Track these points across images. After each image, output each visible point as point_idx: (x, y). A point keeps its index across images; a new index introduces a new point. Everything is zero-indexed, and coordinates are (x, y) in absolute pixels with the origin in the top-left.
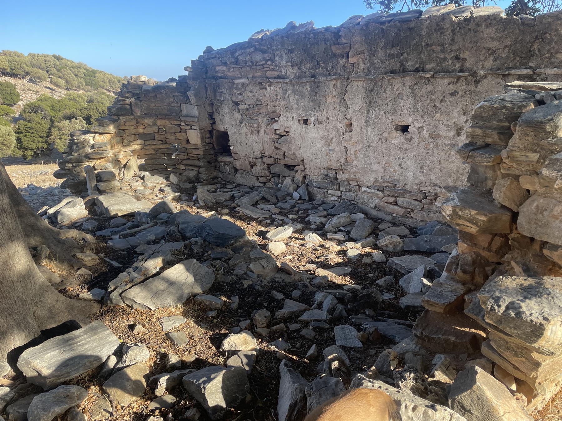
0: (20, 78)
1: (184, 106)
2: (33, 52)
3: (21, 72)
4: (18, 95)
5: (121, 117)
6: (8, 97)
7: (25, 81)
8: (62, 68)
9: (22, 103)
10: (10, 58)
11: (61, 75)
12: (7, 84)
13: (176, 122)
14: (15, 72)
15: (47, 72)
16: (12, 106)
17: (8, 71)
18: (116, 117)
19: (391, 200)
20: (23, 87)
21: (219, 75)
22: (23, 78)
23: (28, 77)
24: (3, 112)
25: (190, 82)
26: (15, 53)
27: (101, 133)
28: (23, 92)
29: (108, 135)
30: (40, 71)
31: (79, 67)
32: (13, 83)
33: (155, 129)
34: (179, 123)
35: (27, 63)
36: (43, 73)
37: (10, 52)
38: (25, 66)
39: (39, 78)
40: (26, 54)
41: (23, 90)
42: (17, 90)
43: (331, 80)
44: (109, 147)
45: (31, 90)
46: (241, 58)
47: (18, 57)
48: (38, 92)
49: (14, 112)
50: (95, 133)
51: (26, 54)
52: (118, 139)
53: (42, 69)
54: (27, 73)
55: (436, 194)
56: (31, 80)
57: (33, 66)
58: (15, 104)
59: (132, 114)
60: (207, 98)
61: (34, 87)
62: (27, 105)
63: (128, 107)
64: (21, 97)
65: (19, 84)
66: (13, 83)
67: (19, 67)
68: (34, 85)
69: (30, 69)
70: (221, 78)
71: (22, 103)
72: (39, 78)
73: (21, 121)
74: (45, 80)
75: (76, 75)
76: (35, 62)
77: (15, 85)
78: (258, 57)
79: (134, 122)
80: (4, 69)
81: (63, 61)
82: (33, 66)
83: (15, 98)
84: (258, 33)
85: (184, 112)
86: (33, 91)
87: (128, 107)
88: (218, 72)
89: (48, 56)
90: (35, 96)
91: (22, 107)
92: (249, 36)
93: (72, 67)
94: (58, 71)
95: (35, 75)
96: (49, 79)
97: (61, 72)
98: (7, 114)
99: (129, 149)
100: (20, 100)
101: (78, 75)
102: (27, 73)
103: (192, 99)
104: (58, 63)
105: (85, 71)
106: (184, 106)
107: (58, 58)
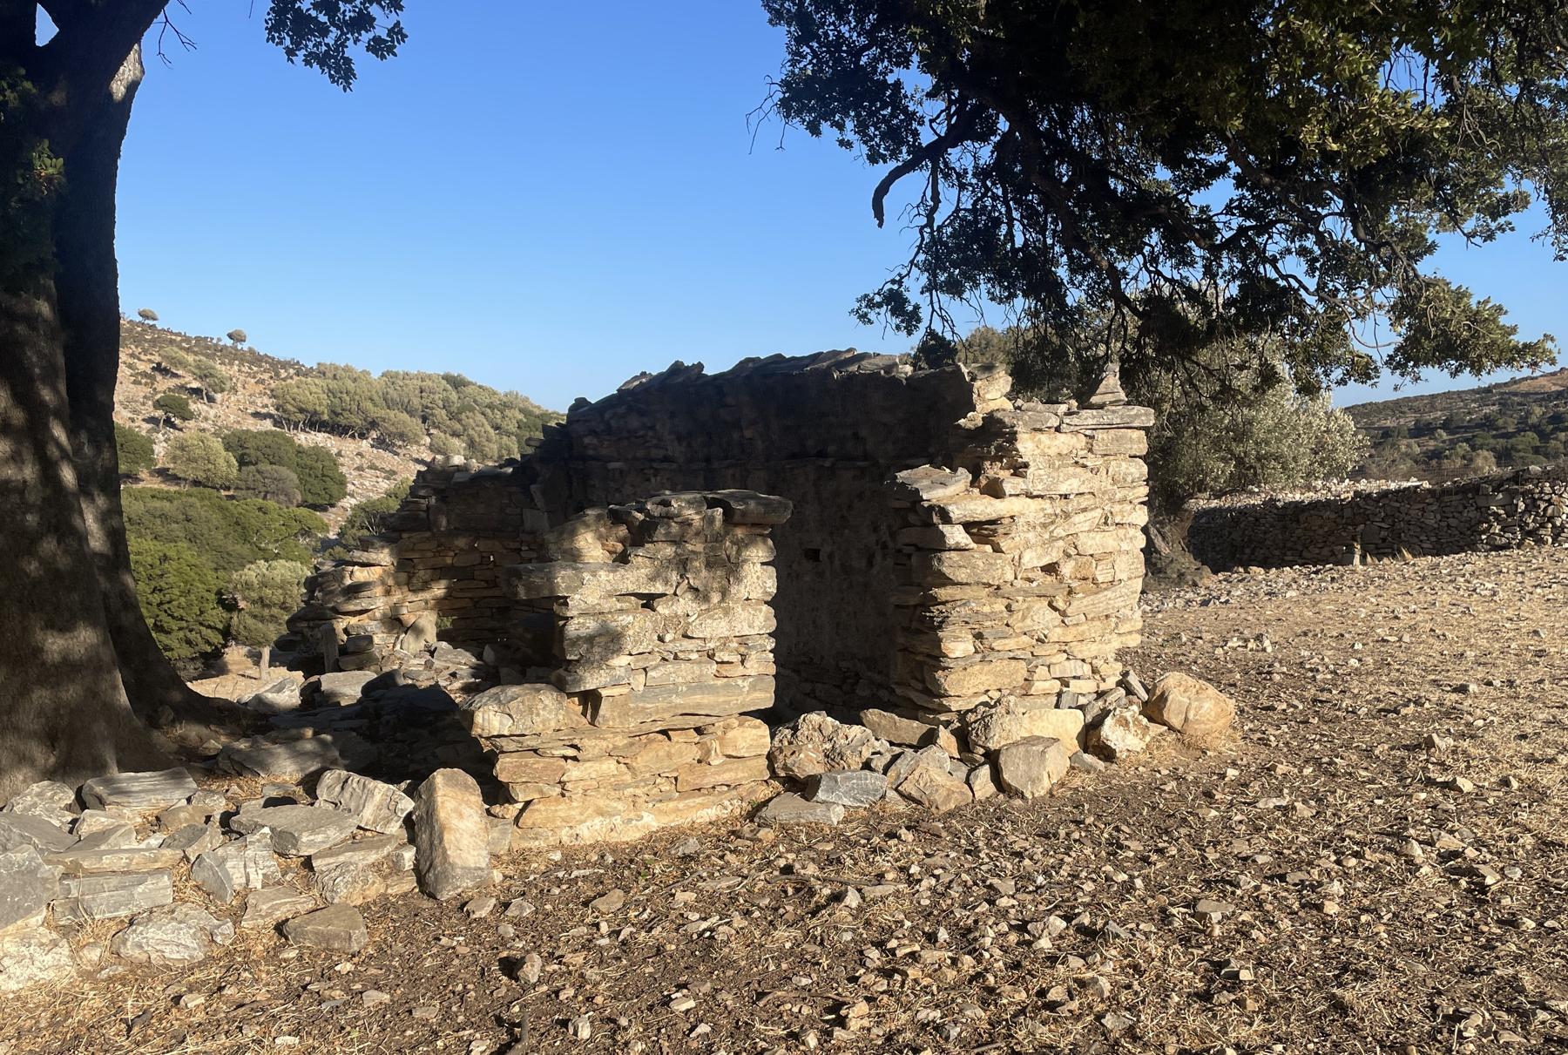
0: (353, 436)
1: (527, 513)
2: (399, 368)
3: (357, 420)
4: (342, 482)
5: (405, 535)
6: (317, 486)
7: (365, 445)
8: (461, 410)
9: (348, 502)
10: (333, 385)
11: (458, 426)
12: (318, 453)
13: (513, 545)
14: (343, 422)
15: (424, 420)
16: (325, 510)
17: (326, 417)
18: (395, 535)
19: (808, 687)
20: (358, 460)
21: (591, 452)
22: (362, 436)
23: (374, 434)
24: (296, 527)
25: (538, 467)
26: (347, 369)
27: (363, 565)
28: (355, 473)
29: (378, 569)
30: (405, 416)
31: (505, 406)
32: (334, 451)
33: (474, 558)
34: (517, 545)
35: (375, 397)
36: (415, 424)
37: (336, 368)
38: (369, 405)
39: (402, 436)
40: (375, 375)
41: (360, 468)
42: (343, 470)
43: (728, 467)
44: (379, 590)
45: (376, 469)
46: (613, 423)
47: (355, 380)
48: (394, 473)
49: (325, 528)
50: (354, 564)
51: (375, 375)
52: (403, 576)
53: (411, 413)
54: (373, 424)
55: (857, 674)
56: (380, 443)
57: (389, 403)
58: (333, 506)
59: (429, 529)
60: (570, 496)
61: (387, 459)
62: (360, 508)
63: (423, 515)
64: (350, 487)
65: (349, 451)
66: (334, 451)
67: (354, 407)
68: (387, 455)
69: (376, 412)
70: (593, 458)
71: (348, 502)
72: (402, 436)
73: (338, 549)
74: (417, 443)
75: (497, 428)
76: (395, 396)
77: (339, 454)
78: (634, 422)
79: (433, 545)
80: (316, 412)
81: (469, 390)
82: (389, 403)
83: (334, 489)
84: (636, 378)
85: (528, 525)
86: (382, 470)
87: (423, 515)
88: (586, 447)
89: (430, 377)
90: (385, 485)
91: (350, 512)
92: (619, 384)
93: (488, 406)
94: (453, 416)
95: (392, 429)
96: (428, 440)
97: (459, 421)
98: (306, 533)
99: (427, 595)
100: (345, 495)
101: (504, 425)
102: (373, 424)
103: (539, 500)
104: (454, 396)
105: (521, 416)
106: (527, 513)
107: (457, 383)
